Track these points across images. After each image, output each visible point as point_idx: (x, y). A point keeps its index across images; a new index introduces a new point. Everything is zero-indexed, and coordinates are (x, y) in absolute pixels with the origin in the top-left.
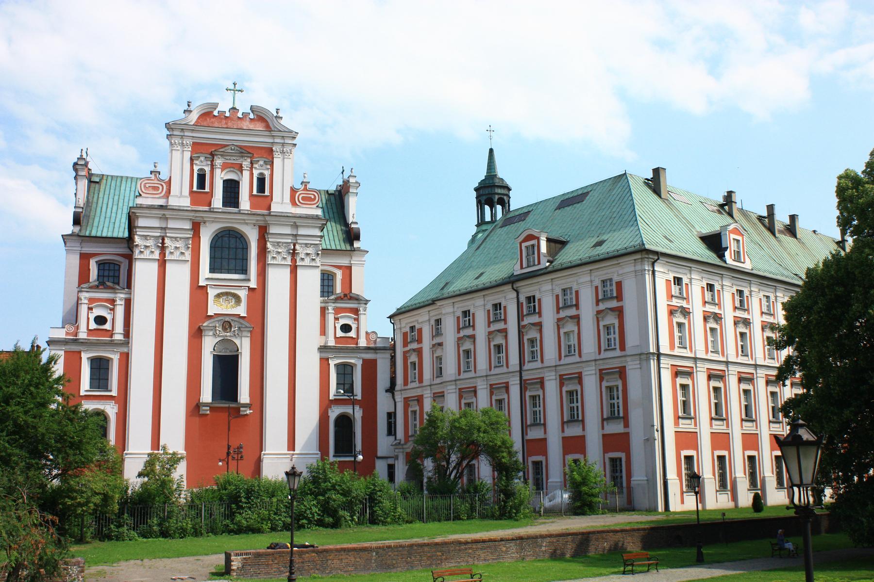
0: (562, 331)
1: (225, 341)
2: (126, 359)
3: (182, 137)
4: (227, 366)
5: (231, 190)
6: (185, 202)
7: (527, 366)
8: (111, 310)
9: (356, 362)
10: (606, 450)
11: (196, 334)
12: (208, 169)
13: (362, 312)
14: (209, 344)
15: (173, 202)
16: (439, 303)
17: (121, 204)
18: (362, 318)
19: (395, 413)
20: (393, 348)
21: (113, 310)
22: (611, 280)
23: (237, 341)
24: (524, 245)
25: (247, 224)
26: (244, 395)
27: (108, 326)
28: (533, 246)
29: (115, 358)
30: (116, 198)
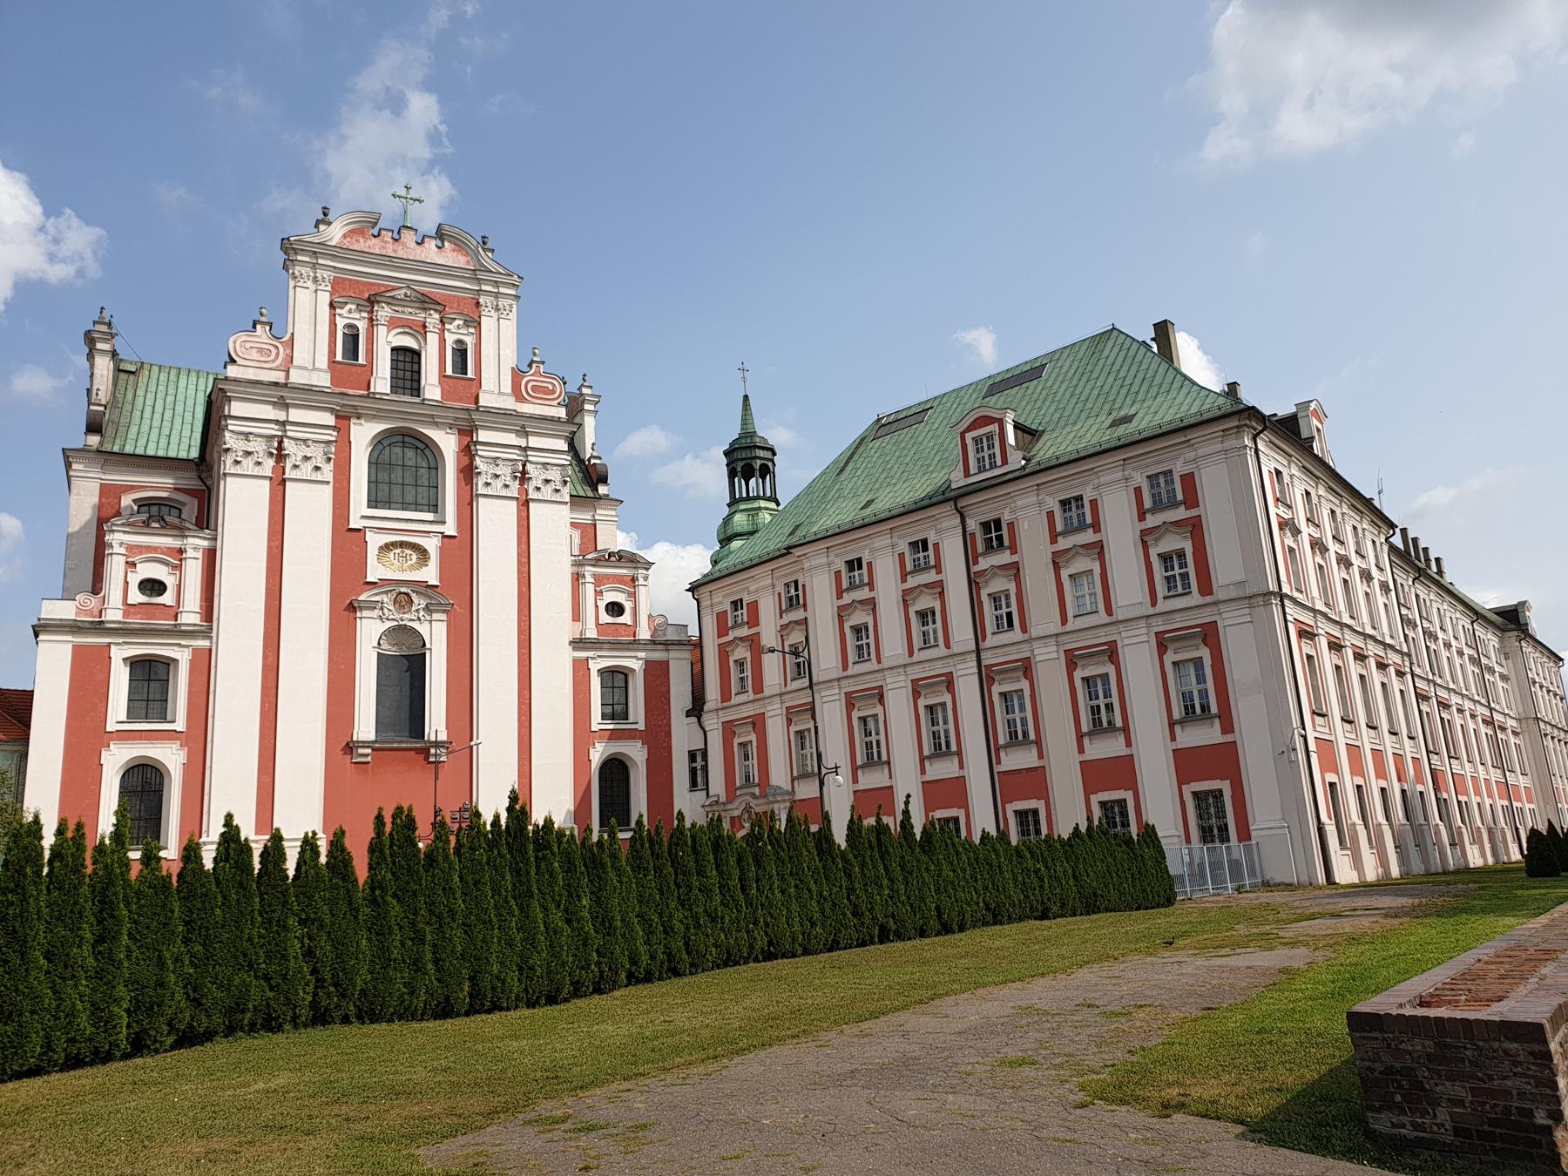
0: (1064, 574)
1: (401, 632)
2: (204, 665)
3: (314, 266)
4: (405, 671)
5: (407, 363)
6: (323, 380)
7: (991, 641)
8: (174, 567)
9: (634, 663)
10: (1182, 780)
11: (345, 611)
12: (362, 326)
13: (641, 581)
14: (370, 632)
15: (296, 377)
16: (797, 552)
17: (179, 409)
18: (642, 591)
19: (705, 752)
20: (699, 645)
21: (178, 568)
22: (1079, 499)
23: (423, 629)
24: (969, 436)
25: (436, 424)
26: (436, 724)
27: (167, 598)
28: (990, 437)
29: (183, 657)
30: (170, 399)
